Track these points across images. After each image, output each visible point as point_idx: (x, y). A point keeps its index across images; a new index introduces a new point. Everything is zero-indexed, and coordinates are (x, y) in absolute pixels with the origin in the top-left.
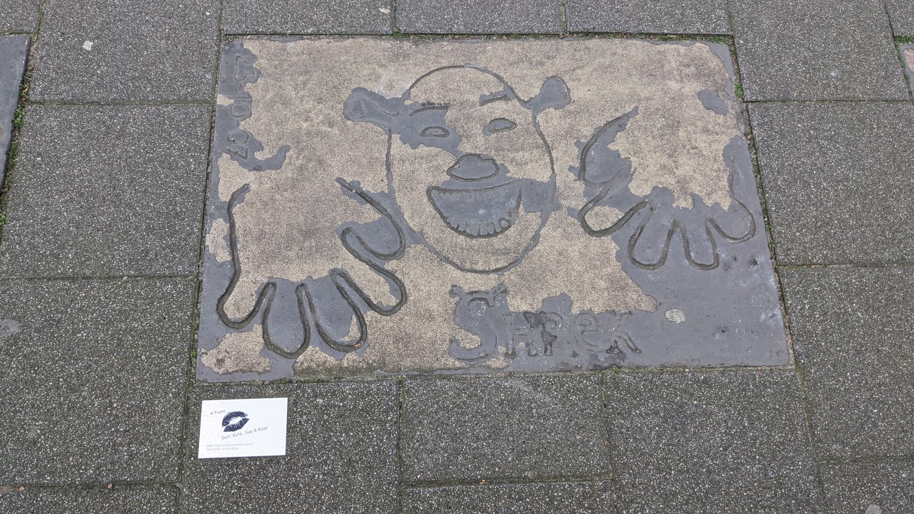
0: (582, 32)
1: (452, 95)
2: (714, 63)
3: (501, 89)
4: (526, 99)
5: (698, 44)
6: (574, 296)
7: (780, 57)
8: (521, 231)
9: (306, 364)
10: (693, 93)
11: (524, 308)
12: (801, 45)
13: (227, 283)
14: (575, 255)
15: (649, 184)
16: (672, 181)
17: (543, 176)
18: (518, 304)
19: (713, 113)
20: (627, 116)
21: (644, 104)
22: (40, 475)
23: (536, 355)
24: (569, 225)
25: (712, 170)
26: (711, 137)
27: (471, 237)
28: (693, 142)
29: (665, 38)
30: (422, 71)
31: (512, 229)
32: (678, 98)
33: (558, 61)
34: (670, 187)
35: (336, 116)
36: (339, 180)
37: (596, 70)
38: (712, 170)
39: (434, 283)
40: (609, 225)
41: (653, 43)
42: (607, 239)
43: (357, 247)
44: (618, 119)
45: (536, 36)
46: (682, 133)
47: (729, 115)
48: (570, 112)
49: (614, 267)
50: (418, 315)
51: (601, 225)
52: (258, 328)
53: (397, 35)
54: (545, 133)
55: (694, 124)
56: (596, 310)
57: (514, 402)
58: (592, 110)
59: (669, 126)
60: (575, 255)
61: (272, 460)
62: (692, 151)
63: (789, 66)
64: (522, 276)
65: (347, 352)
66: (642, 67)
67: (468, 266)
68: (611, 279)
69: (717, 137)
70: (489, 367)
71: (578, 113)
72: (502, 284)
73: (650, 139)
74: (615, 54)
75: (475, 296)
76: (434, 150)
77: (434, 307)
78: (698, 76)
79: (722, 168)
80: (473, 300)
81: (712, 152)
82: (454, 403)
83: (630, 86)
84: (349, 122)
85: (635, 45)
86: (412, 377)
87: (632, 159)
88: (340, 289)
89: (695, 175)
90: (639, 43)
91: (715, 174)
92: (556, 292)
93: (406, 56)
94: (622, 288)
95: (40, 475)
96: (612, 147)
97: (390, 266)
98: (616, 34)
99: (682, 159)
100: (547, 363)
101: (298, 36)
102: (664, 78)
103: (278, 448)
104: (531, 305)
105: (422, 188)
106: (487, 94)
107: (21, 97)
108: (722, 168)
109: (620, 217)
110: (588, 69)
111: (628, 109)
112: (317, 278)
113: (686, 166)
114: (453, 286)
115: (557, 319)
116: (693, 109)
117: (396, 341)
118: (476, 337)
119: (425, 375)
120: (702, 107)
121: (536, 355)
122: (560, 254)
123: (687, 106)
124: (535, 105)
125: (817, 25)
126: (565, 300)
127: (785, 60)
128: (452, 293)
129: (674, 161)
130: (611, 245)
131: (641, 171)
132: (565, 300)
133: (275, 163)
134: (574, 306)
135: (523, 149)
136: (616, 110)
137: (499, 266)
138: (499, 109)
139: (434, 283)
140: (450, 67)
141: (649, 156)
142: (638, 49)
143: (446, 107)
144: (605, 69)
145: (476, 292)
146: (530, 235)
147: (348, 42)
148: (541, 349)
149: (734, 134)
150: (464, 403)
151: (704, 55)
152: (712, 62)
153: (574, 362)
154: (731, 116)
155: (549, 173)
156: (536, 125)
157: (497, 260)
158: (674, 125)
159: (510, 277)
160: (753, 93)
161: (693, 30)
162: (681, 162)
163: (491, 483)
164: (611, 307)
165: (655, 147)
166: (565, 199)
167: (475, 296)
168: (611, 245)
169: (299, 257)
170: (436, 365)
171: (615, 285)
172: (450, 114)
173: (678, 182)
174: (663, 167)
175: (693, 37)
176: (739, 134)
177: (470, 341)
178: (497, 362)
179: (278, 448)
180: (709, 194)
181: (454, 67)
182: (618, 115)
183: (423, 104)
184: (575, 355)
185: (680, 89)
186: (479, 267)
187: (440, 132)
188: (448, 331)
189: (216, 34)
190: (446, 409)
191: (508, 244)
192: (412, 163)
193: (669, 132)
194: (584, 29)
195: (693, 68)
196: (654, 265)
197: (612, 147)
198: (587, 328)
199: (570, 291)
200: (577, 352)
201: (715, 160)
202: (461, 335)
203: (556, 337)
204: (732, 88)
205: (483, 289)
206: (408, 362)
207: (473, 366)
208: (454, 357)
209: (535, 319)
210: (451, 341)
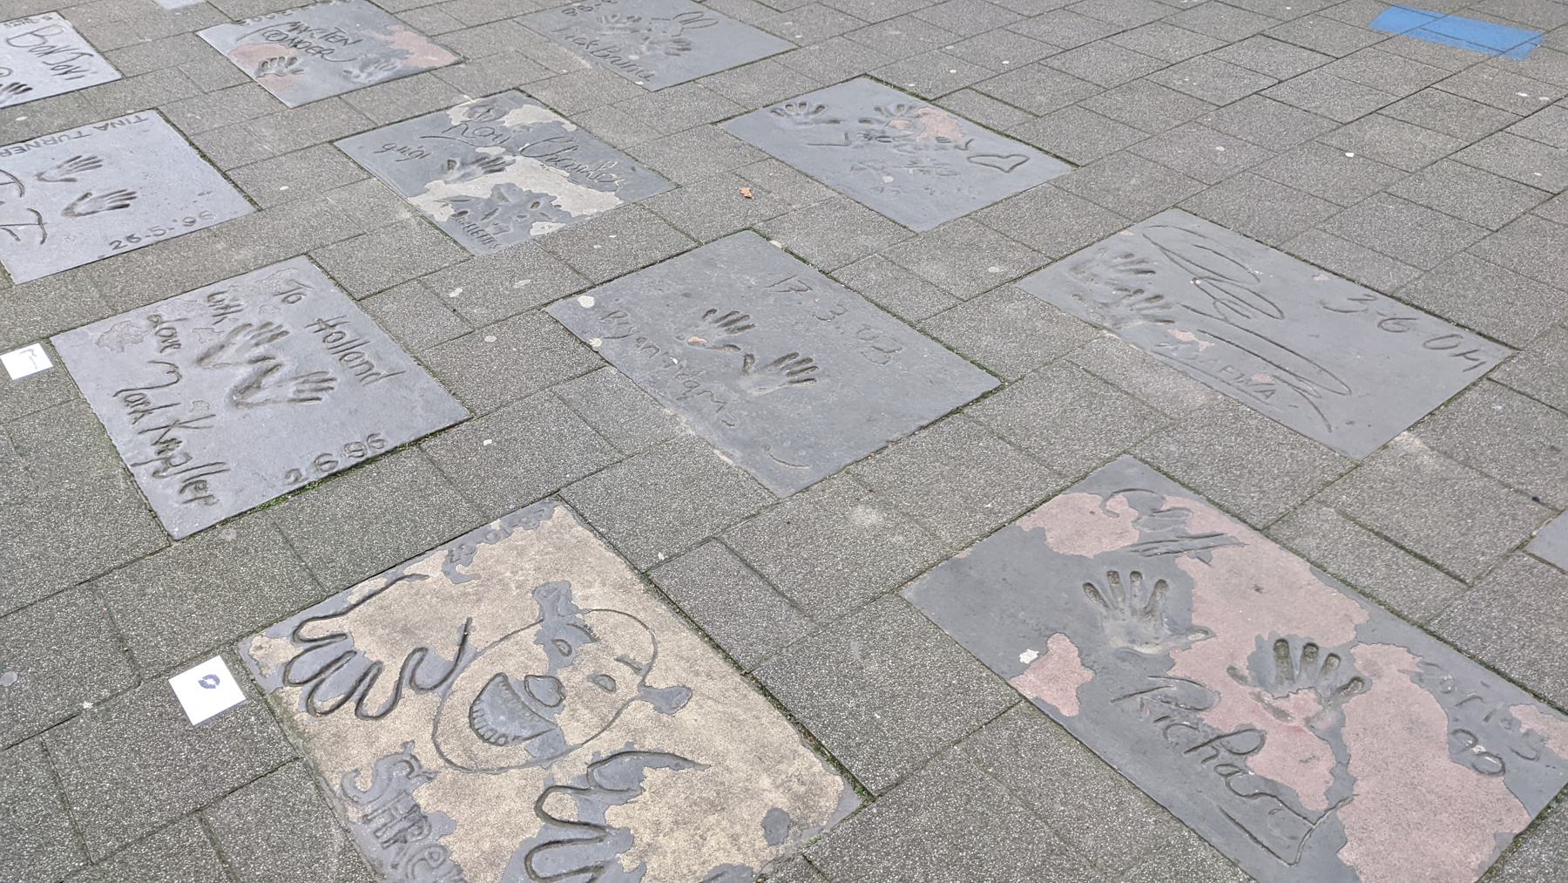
0: (760, 683)
1: (610, 638)
2: (828, 803)
3: (644, 663)
4: (648, 684)
5: (838, 778)
6: (460, 832)
7: (888, 854)
8: (502, 756)
9: (283, 695)
10: (771, 804)
11: (422, 802)
12: (924, 865)
13: (331, 613)
14: (505, 808)
15: (627, 821)
16: (647, 839)
17: (572, 739)
18: (423, 796)
19: (761, 833)
20: (694, 764)
21: (719, 769)
22: (119, 611)
23: (378, 837)
24: (534, 786)
25: (688, 866)
26: (729, 846)
27: (471, 725)
28: (709, 833)
29: (818, 748)
30: (620, 607)
31: (499, 748)
32: (751, 794)
33: (710, 683)
34: (637, 841)
35: (530, 585)
36: (469, 620)
37: (724, 713)
38: (688, 866)
39: (408, 727)
40: (557, 816)
41: (802, 741)
42: (540, 822)
43: (412, 663)
44: (685, 760)
45: (727, 657)
46: (712, 819)
47: (774, 849)
48: (659, 720)
49: (511, 844)
50: (369, 735)
51: (552, 809)
52: (301, 650)
53: (644, 576)
54: (622, 716)
55: (732, 823)
56: (455, 857)
57: (317, 845)
58: (676, 734)
59: (712, 804)
60: (505, 808)
61: (186, 721)
62: (697, 838)
63: (884, 868)
64: (455, 782)
65: (308, 711)
66: (763, 746)
67: (440, 740)
68: (496, 851)
69: (734, 851)
70: (345, 810)
71: (664, 726)
72: (436, 773)
73: (683, 796)
74: (758, 718)
75: (413, 761)
76: (544, 655)
77: (384, 740)
78: (797, 797)
79: (698, 874)
80: (407, 762)
81: (710, 855)
82: (294, 804)
83: (730, 747)
84: (530, 595)
85: (785, 728)
86: (306, 765)
87: (646, 794)
88: (365, 675)
89: (669, 855)
90: (791, 730)
91: (685, 871)
92: (455, 815)
93: (627, 591)
94: (492, 864)
95: (119, 611)
96: (647, 771)
97: (407, 691)
98: (781, 707)
99: (680, 834)
100: (373, 849)
101: (592, 527)
102: (767, 770)
103: (196, 717)
104: (428, 804)
105: (499, 669)
106: (631, 657)
107: (419, 440)
108: (698, 874)
109: (572, 820)
110: (720, 707)
111: (701, 761)
112: (1050, 645)
113: (675, 842)
114: (413, 742)
115: (426, 832)
116: (751, 814)
117: (335, 735)
118: (370, 784)
119: (313, 772)
120: (760, 819)
121: (378, 837)
122: (498, 797)
123: (749, 806)
124: (646, 692)
125: (968, 867)
126: (449, 826)
127: (888, 860)
128: (405, 744)
129: (672, 830)
130: (535, 829)
131: (637, 808)
132: (449, 826)
133: (458, 579)
134: (447, 838)
135: (592, 710)
136: (692, 752)
137: (454, 760)
138: (623, 674)
139: (408, 727)
140: (639, 621)
141: (661, 805)
142: (781, 732)
143: (594, 640)
144: (732, 719)
145: (416, 760)
146: (503, 764)
147: (611, 554)
148: (385, 838)
149: (752, 865)
150: (299, 811)
151: (829, 789)
152: (827, 801)
153: (388, 870)
154: (774, 852)
155: (579, 742)
156: (626, 705)
157: (459, 756)
158: (714, 807)
159: (448, 774)
160: (817, 853)
161: (847, 763)
162: (676, 834)
163: (227, 872)
164: (465, 866)
165: (676, 805)
166: (559, 767)
167: (413, 761)
168: (535, 829)
169: (380, 637)
170: (327, 774)
171: (492, 859)
172: (591, 646)
173: (649, 845)
174: (657, 823)
175: (842, 769)
176: (757, 869)
177: (364, 783)
178: (354, 814)
179: (196, 717)
180: (655, 878)
181: (642, 624)
182: (689, 757)
183: (586, 626)
184: (395, 867)
185: (764, 790)
186: (443, 748)
187: (417, 656)
188: (365, 761)
189: (554, 489)
190: (286, 801)
191: (481, 754)
192: (519, 650)
193: (704, 807)
194: (765, 682)
195: (803, 789)
196: (537, 877)
197: (647, 771)
198: (430, 861)
199: (462, 826)
200: (399, 867)
201: (704, 863)
202: (367, 773)
203: (406, 842)
204: (812, 836)
205: (423, 762)
206: (319, 754)
207: (340, 799)
208: (342, 781)
209: (417, 817)
210: (356, 770)
